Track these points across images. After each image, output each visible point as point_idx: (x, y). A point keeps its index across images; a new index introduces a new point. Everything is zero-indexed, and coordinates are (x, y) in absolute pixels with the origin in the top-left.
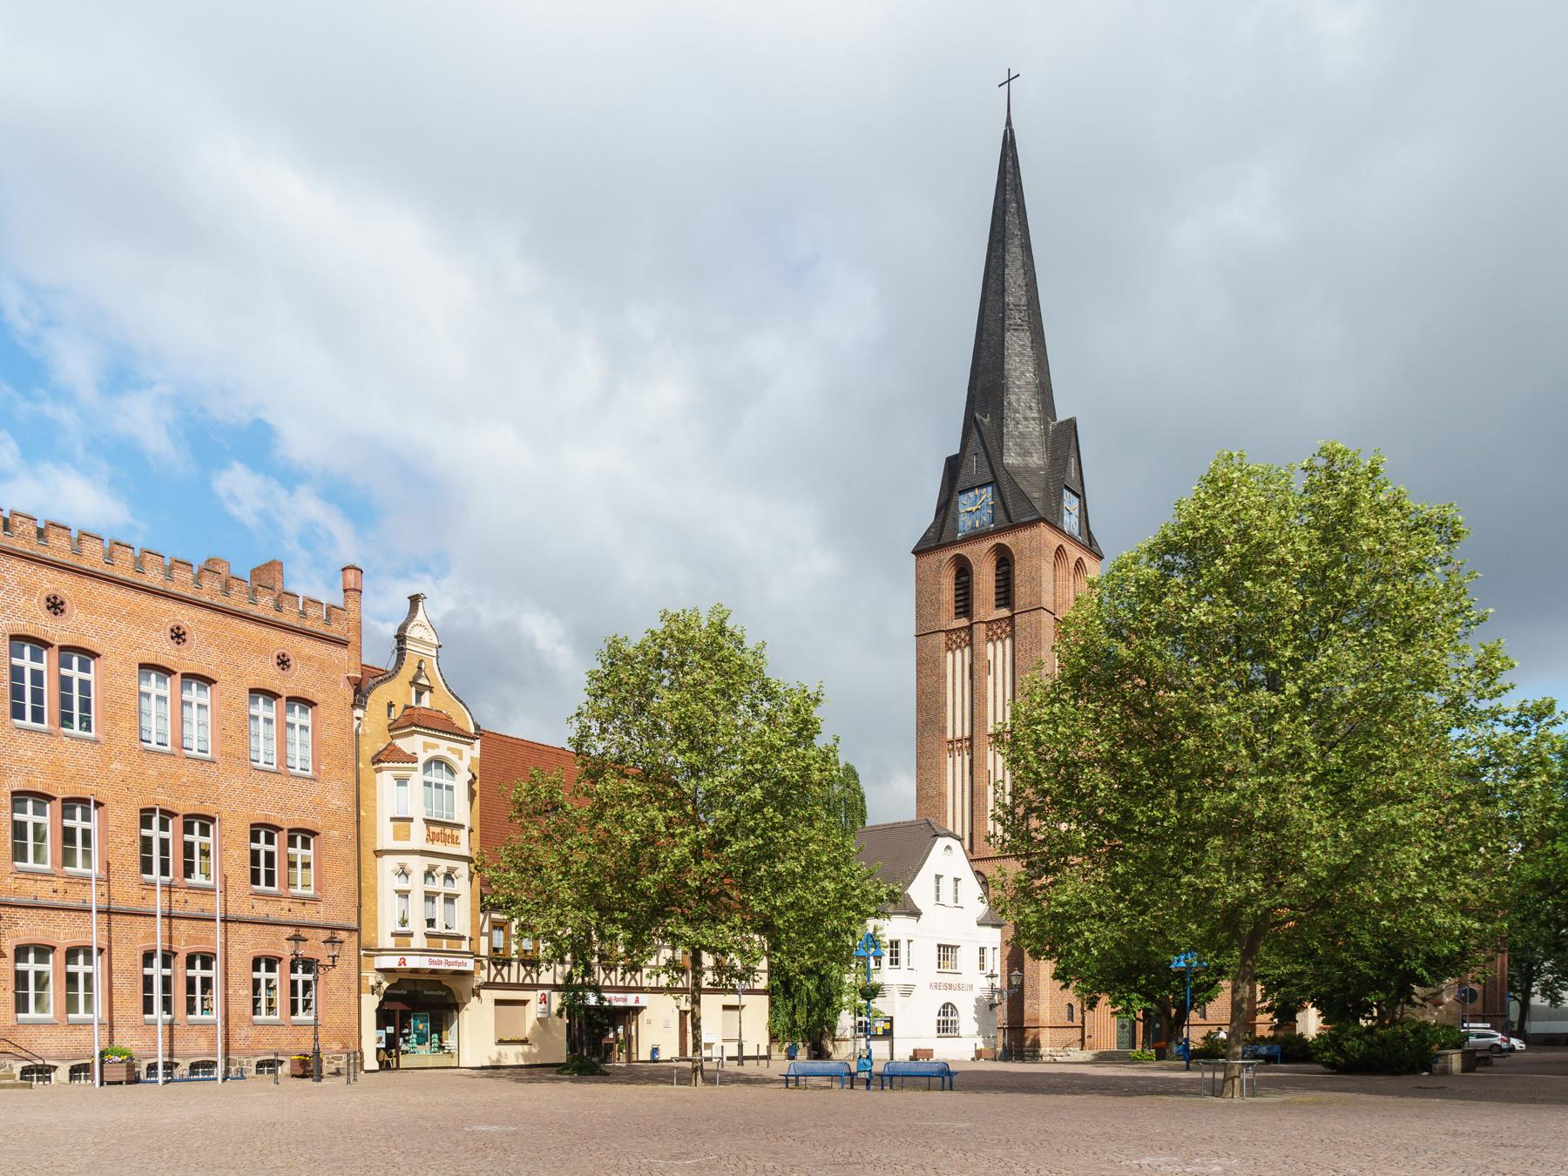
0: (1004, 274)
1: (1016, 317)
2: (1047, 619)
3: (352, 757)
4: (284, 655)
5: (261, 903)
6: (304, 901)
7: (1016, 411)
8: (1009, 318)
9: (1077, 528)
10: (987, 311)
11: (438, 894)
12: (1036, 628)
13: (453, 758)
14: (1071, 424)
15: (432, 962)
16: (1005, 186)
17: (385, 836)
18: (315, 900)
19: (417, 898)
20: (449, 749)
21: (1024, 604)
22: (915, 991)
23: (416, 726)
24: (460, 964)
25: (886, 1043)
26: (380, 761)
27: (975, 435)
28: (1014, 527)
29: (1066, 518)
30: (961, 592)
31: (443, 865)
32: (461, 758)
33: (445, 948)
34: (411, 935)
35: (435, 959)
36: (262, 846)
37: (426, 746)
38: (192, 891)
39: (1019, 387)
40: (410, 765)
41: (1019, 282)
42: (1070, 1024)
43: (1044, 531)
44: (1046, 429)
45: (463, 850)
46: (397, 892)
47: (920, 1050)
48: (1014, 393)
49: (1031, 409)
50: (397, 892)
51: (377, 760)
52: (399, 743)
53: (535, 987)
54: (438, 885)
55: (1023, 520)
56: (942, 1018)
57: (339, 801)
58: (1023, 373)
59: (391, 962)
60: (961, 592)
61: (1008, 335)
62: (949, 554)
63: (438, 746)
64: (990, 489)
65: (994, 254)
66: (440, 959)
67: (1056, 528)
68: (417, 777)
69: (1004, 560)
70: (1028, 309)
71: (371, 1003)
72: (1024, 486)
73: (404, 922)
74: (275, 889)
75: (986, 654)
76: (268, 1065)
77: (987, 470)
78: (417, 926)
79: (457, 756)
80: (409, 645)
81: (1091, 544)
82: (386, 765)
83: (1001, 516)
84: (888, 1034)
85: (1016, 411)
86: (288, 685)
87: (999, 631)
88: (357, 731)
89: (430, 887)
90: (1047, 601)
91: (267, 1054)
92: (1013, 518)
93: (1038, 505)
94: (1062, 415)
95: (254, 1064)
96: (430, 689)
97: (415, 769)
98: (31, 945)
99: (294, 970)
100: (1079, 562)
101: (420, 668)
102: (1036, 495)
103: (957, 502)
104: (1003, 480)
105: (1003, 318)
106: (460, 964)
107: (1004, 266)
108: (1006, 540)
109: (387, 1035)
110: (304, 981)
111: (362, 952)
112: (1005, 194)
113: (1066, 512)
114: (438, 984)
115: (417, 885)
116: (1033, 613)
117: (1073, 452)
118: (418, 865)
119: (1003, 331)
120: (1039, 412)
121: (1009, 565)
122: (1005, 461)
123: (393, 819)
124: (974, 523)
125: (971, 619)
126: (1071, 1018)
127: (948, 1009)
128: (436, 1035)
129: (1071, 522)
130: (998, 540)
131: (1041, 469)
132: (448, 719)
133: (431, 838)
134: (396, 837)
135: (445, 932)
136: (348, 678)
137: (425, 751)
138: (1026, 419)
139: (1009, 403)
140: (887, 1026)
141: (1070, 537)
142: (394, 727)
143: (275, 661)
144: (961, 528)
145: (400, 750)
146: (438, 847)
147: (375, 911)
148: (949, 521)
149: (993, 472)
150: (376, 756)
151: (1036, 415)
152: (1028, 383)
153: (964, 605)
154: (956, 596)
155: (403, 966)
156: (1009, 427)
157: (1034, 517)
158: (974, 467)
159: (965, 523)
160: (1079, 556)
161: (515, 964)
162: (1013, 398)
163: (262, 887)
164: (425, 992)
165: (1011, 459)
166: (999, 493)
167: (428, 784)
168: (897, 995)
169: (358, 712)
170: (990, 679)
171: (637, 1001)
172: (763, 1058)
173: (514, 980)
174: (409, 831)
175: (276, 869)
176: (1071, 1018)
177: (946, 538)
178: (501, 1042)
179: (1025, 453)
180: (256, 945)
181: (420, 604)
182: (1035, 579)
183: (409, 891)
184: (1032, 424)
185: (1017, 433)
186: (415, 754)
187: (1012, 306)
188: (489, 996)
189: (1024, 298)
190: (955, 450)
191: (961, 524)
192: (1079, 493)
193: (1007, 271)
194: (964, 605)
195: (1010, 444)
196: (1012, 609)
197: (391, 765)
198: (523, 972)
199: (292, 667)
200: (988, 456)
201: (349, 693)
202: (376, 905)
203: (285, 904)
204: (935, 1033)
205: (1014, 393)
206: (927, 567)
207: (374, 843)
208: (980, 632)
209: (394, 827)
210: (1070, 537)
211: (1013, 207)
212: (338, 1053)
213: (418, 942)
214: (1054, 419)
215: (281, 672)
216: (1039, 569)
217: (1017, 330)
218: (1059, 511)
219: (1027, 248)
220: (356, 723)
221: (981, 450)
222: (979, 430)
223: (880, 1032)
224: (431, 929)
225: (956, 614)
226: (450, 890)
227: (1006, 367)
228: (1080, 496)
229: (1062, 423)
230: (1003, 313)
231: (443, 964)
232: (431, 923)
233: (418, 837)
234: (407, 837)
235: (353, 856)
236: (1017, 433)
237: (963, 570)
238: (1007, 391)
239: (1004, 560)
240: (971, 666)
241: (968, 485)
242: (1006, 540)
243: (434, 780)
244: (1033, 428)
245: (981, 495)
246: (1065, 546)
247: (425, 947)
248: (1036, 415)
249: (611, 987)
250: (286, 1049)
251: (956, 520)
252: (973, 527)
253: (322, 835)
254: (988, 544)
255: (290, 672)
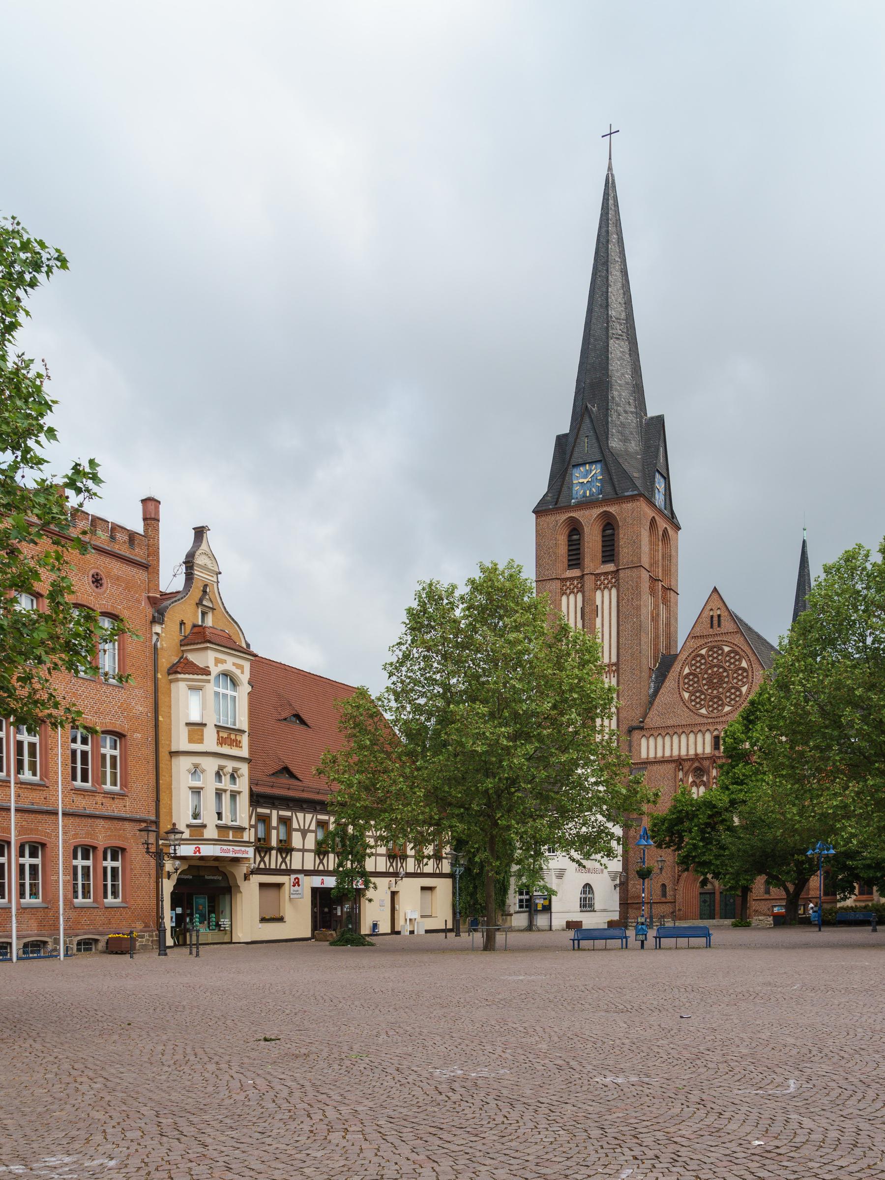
0: (608, 292)
1: (617, 328)
2: (645, 575)
3: (151, 668)
4: (97, 575)
5: (80, 798)
6: (112, 796)
7: (618, 405)
8: (612, 329)
9: (663, 503)
10: (594, 321)
11: (225, 791)
12: (637, 583)
13: (238, 672)
14: (659, 421)
15: (222, 851)
16: (608, 220)
17: (181, 740)
18: (122, 796)
19: (209, 797)
20: (234, 664)
21: (627, 562)
22: (567, 873)
23: (210, 642)
24: (243, 852)
25: (547, 916)
26: (177, 672)
27: (587, 421)
28: (618, 498)
29: (657, 496)
30: (574, 547)
31: (230, 765)
32: (242, 673)
33: (231, 838)
34: (205, 826)
35: (225, 847)
36: (79, 747)
37: (218, 661)
38: (24, 786)
39: (620, 386)
40: (204, 677)
41: (619, 300)
42: (663, 900)
43: (642, 505)
44: (641, 422)
45: (244, 752)
46: (190, 788)
47: (572, 922)
48: (617, 390)
49: (629, 403)
50: (190, 788)
51: (173, 670)
52: (191, 657)
53: (288, 872)
54: (226, 784)
55: (626, 494)
56: (583, 896)
57: (141, 707)
58: (623, 374)
59: (186, 850)
60: (574, 547)
61: (611, 342)
62: (564, 517)
63: (225, 662)
64: (599, 466)
65: (599, 274)
66: (229, 847)
67: (652, 504)
68: (211, 688)
69: (609, 526)
70: (627, 323)
71: (168, 886)
72: (626, 466)
73: (196, 816)
74: (88, 785)
75: (595, 601)
76: (86, 945)
77: (597, 450)
78: (209, 818)
79: (240, 671)
80: (197, 572)
81: (673, 518)
82: (182, 676)
83: (608, 489)
84: (547, 909)
85: (618, 405)
86: (101, 602)
87: (606, 582)
88: (155, 645)
89: (221, 786)
90: (645, 561)
91: (85, 934)
92: (619, 492)
93: (638, 483)
94: (652, 412)
95: (75, 943)
96: (213, 609)
97: (208, 681)
98: (27, 842)
99: (22, 855)
100: (665, 531)
101: (205, 592)
102: (636, 475)
103: (572, 474)
104: (610, 460)
105: (607, 328)
106: (243, 852)
107: (608, 286)
108: (612, 509)
109: (176, 914)
110: (30, 865)
111: (161, 842)
112: (608, 227)
113: (656, 491)
114: (216, 870)
115: (210, 785)
116: (635, 570)
117: (662, 444)
118: (210, 765)
119: (607, 338)
120: (636, 407)
121: (613, 529)
122: (610, 445)
123: (188, 724)
124: (585, 493)
125: (583, 571)
126: (664, 894)
127: (588, 889)
128: (213, 915)
129: (659, 499)
130: (605, 509)
131: (637, 454)
132: (230, 638)
133: (221, 742)
134: (191, 741)
135: (230, 824)
136: (149, 598)
137: (216, 665)
138: (626, 412)
139: (613, 397)
140: (546, 903)
141: (660, 511)
142: (185, 642)
143: (91, 579)
144: (574, 496)
145: (192, 663)
146: (226, 750)
147: (171, 805)
148: (565, 488)
149: (602, 452)
150: (171, 668)
151: (633, 410)
152: (627, 383)
153: (575, 558)
154: (569, 551)
155: (197, 854)
156: (613, 417)
157: (636, 492)
158: (586, 446)
159: (578, 491)
160: (665, 526)
161: (274, 852)
162: (616, 393)
163: (79, 783)
164: (207, 877)
165: (614, 443)
166: (607, 470)
167: (217, 694)
168: (554, 877)
169: (157, 629)
170: (598, 621)
171: (322, 883)
172: (451, 930)
173: (273, 866)
174: (202, 735)
175: (90, 767)
176: (664, 894)
177: (562, 502)
178: (263, 920)
179: (625, 440)
180: (76, 835)
181: (205, 535)
182: (636, 544)
183: (202, 788)
184: (631, 417)
185: (619, 423)
186: (208, 667)
187: (614, 319)
188: (256, 879)
189: (624, 314)
190: (565, 429)
191: (574, 492)
192: (665, 475)
193: (610, 290)
194: (575, 558)
195: (614, 431)
196: (617, 565)
197: (187, 676)
198: (280, 860)
199: (105, 586)
200: (597, 439)
201: (150, 611)
202: (171, 800)
203: (99, 798)
204: (579, 909)
205: (617, 390)
206: (545, 525)
207: (170, 745)
208: (589, 582)
209: (189, 731)
210: (660, 511)
211: (614, 238)
212: (141, 931)
213: (211, 832)
214: (646, 414)
215: (95, 588)
216: (639, 535)
217: (618, 339)
218: (652, 489)
219: (625, 273)
220: (155, 638)
221: (592, 433)
222: (590, 417)
223: (540, 907)
224: (220, 822)
225: (569, 566)
226: (235, 788)
227: (610, 368)
228: (667, 479)
229: (652, 418)
230: (607, 324)
231: (230, 851)
232: (219, 815)
233: (210, 742)
234: (201, 741)
235: (152, 757)
236: (619, 423)
237: (575, 530)
238: (611, 388)
239: (609, 526)
240: (582, 609)
241: (580, 461)
242: (612, 509)
243: (221, 690)
244: (632, 420)
245: (591, 471)
246: (657, 518)
247: (216, 837)
248: (633, 410)
249: (265, 869)
250: (101, 929)
251: (570, 489)
252: (584, 496)
253: (128, 737)
254: (596, 512)
255: (103, 590)
